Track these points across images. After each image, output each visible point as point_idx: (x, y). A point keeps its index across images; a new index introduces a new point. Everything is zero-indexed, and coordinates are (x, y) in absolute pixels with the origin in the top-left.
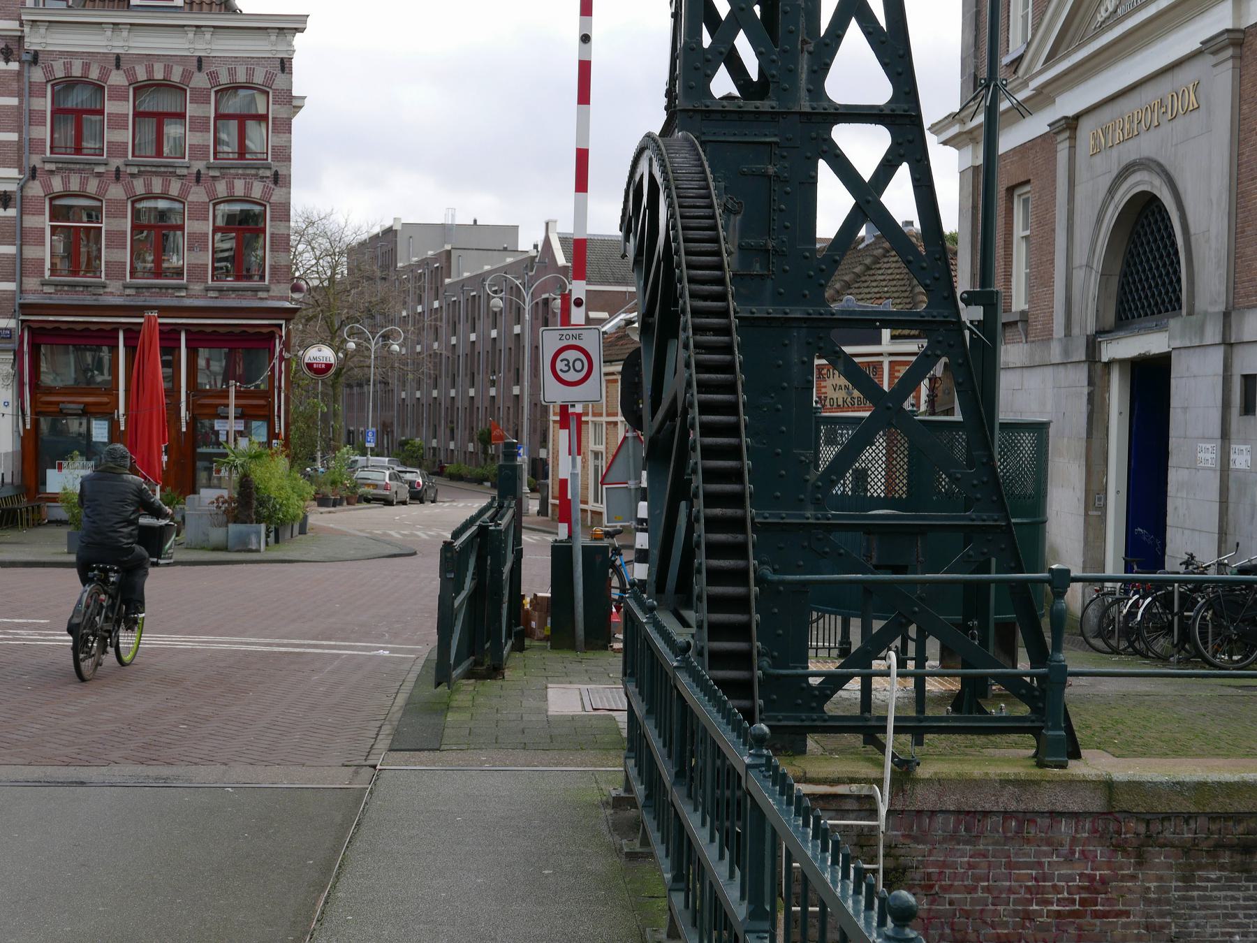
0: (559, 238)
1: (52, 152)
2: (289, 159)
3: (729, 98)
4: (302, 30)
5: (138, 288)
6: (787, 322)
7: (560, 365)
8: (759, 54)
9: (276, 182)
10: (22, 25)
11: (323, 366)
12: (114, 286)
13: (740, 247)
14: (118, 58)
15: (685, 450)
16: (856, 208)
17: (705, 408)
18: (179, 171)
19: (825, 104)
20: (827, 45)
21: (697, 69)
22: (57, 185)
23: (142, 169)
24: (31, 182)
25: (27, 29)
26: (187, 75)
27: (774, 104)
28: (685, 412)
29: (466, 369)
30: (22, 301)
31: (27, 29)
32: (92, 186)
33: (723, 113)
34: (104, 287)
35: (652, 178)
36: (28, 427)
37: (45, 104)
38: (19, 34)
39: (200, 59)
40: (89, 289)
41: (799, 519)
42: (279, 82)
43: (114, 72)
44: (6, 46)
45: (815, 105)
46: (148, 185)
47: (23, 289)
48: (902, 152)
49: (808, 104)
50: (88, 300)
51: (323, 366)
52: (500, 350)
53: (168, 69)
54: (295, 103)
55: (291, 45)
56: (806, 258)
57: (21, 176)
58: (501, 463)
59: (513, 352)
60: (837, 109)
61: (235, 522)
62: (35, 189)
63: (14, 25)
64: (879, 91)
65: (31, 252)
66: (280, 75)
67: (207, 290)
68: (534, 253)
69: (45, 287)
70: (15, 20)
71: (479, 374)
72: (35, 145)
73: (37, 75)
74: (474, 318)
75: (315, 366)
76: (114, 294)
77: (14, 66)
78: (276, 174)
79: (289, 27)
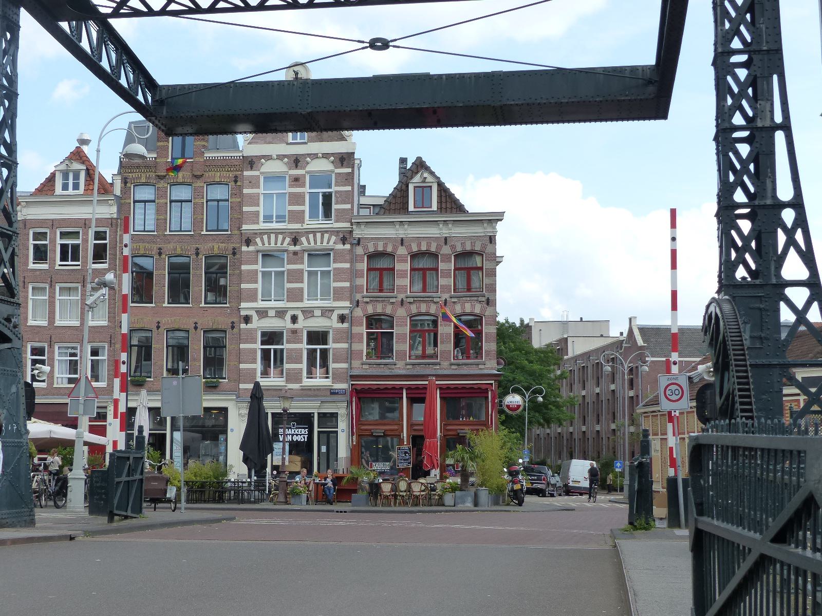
0: (638, 328)
1: (367, 292)
2: (495, 291)
3: (744, 278)
4: (501, 220)
6: (770, 366)
7: (668, 392)
8: (755, 262)
9: (488, 304)
10: (352, 225)
11: (516, 406)
12: (400, 364)
13: (751, 337)
14: (402, 240)
15: (734, 403)
16: (797, 320)
17: (740, 390)
18: (435, 300)
19: (782, 280)
20: (781, 257)
21: (730, 269)
23: (415, 299)
24: (356, 308)
25: (354, 227)
26: (439, 247)
27: (761, 281)
28: (733, 392)
29: (580, 414)
30: (351, 374)
31: (354, 227)
32: (389, 310)
33: (743, 284)
34: (395, 365)
35: (716, 314)
36: (354, 443)
37: (364, 266)
38: (351, 229)
39: (446, 239)
40: (387, 366)
42: (489, 249)
43: (400, 247)
44: (344, 236)
45: (778, 280)
47: (352, 367)
48: (814, 297)
49: (775, 280)
50: (387, 372)
51: (516, 406)
52: (602, 401)
53: (429, 245)
54: (498, 260)
55: (494, 228)
56: (777, 340)
57: (351, 306)
58: (641, 439)
59: (610, 401)
60: (786, 282)
62: (358, 312)
63: (347, 225)
64: (803, 273)
65: (356, 347)
66: (489, 245)
67: (451, 364)
68: (622, 338)
69: (363, 366)
70: (348, 222)
71: (588, 416)
72: (358, 289)
73: (359, 250)
74: (584, 381)
75: (511, 406)
76: (401, 367)
77: (348, 246)
78: (488, 300)
79: (494, 219)
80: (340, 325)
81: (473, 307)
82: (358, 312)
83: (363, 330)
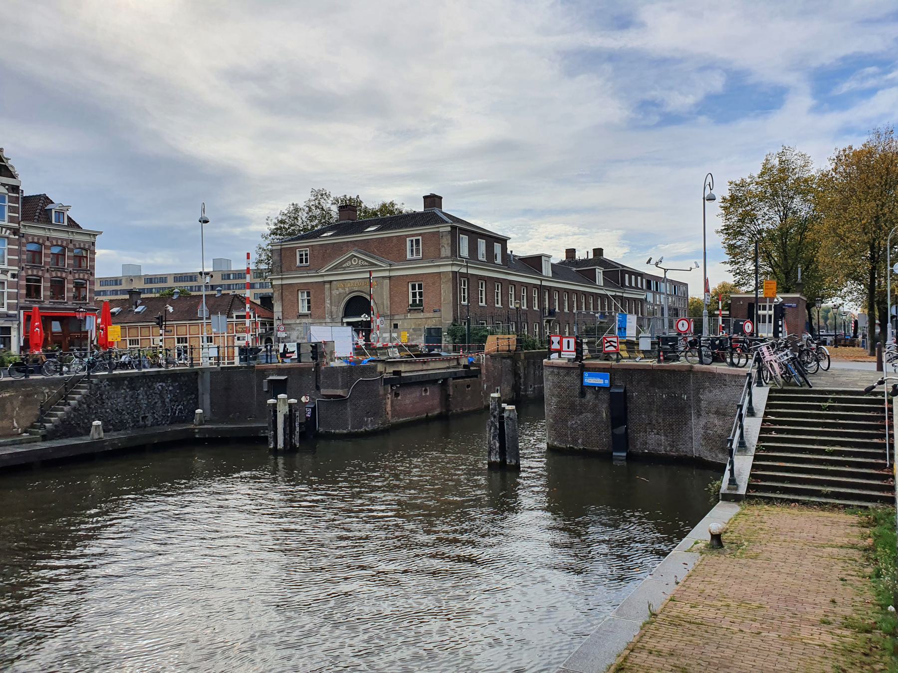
5: (54, 303)
22: (30, 272)
32: (40, 273)
41: (818, 410)
46: (56, 274)
61: (517, 340)
62: (23, 273)
63: (17, 225)
73: (24, 240)
77: (17, 237)
80: (12, 279)
81: (38, 272)
82: (23, 273)
83: (24, 283)
